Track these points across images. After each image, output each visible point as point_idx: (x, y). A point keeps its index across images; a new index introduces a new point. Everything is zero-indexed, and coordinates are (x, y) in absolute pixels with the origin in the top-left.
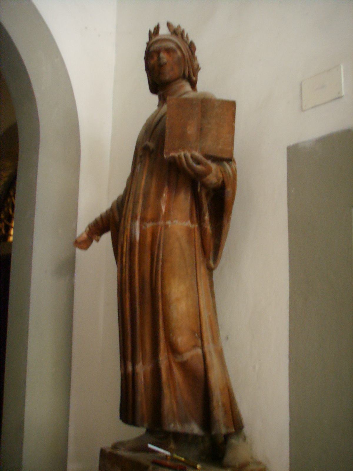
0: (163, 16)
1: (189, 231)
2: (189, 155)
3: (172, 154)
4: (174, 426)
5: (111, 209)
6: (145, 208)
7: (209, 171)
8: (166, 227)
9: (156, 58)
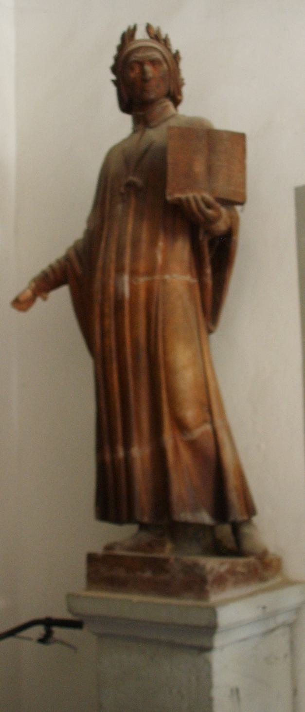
0: (139, 16)
1: (190, 286)
2: (199, 197)
3: (178, 195)
4: (186, 516)
5: (67, 258)
6: (135, 258)
7: (219, 217)
8: (164, 282)
9: (137, 70)
